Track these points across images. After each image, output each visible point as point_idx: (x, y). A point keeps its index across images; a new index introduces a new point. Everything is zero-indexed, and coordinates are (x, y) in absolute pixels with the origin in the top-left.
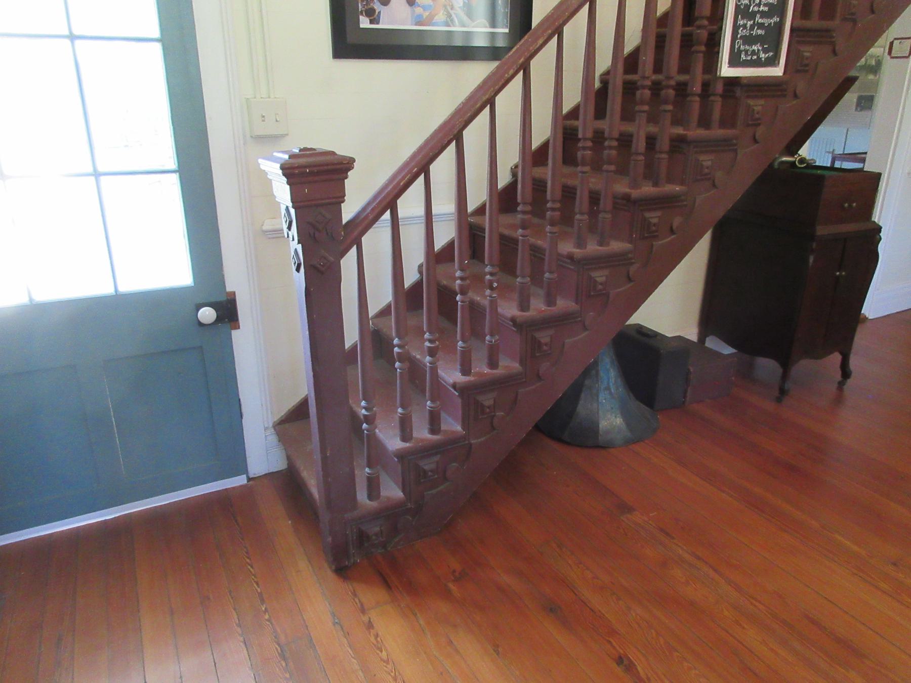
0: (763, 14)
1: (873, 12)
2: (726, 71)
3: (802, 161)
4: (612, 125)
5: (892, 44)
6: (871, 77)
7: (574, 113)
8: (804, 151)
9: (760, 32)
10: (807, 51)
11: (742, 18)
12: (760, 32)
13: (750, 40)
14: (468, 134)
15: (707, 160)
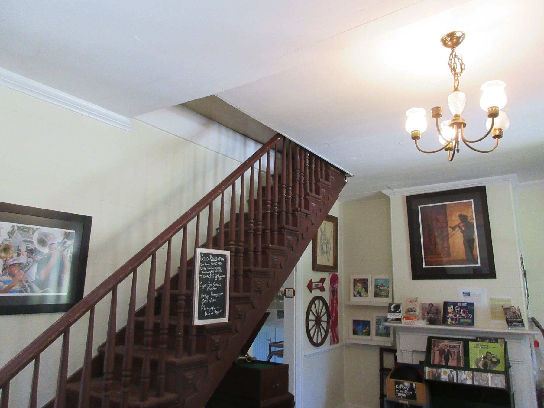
0: (214, 292)
1: (268, 286)
2: (197, 322)
3: (249, 358)
4: (166, 320)
5: (285, 290)
6: (281, 301)
7: (142, 312)
8: (251, 353)
9: (213, 300)
10: (240, 308)
11: (204, 294)
12: (213, 300)
13: (208, 305)
14: (120, 287)
15: (189, 375)
